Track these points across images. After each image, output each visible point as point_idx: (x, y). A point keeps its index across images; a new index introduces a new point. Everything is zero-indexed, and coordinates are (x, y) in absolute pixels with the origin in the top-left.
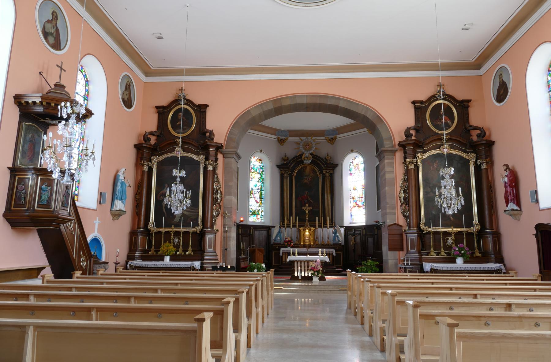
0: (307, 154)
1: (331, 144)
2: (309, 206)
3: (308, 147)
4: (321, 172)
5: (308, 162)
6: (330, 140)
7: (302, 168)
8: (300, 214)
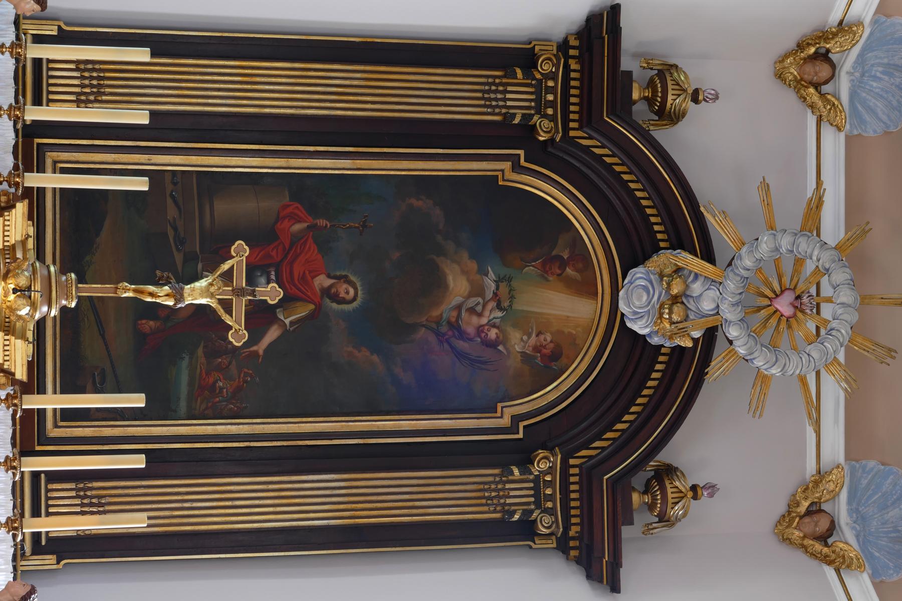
0: (713, 297)
1: (787, 518)
2: (260, 316)
3: (784, 305)
4: (546, 433)
5: (640, 303)
6: (815, 510)
7: (581, 256)
8: (167, 228)
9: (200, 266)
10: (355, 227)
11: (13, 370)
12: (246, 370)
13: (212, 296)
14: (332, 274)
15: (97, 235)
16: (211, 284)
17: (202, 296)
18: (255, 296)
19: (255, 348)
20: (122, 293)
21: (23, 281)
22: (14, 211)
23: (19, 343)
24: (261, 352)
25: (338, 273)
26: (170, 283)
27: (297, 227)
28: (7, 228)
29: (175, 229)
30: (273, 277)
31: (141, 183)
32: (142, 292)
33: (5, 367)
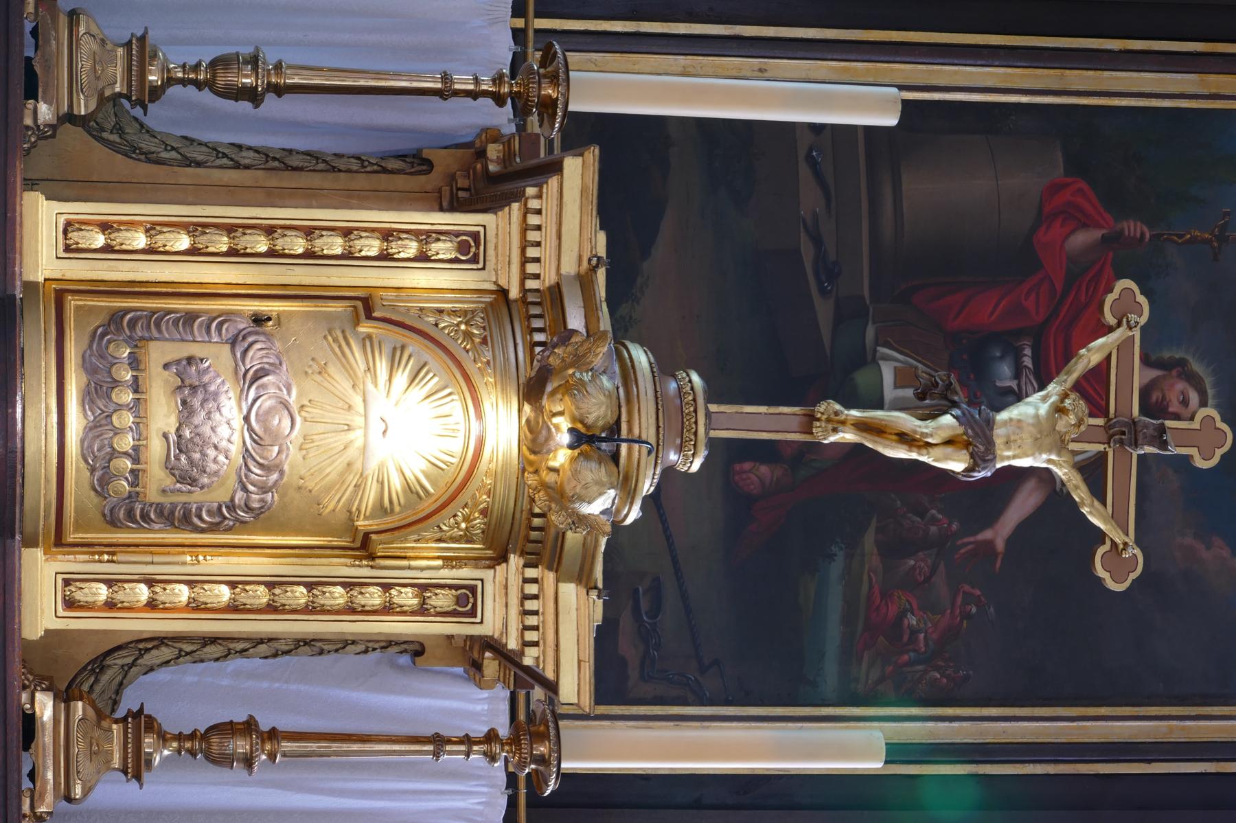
2: (1171, 496)
9: (870, 332)
10: (1208, 242)
11: (550, 674)
12: (967, 588)
13: (1060, 445)
14: (1153, 357)
15: (645, 253)
16: (1059, 410)
17: (1038, 447)
18: (1164, 445)
19: (987, 535)
20: (826, 434)
21: (597, 411)
22: (553, 182)
23: (569, 591)
24: (1000, 545)
25: (1166, 355)
26: (955, 404)
27: (1081, 239)
28: (533, 236)
29: (817, 241)
30: (1028, 362)
31: (880, 105)
32: (877, 430)
33: (528, 661)
